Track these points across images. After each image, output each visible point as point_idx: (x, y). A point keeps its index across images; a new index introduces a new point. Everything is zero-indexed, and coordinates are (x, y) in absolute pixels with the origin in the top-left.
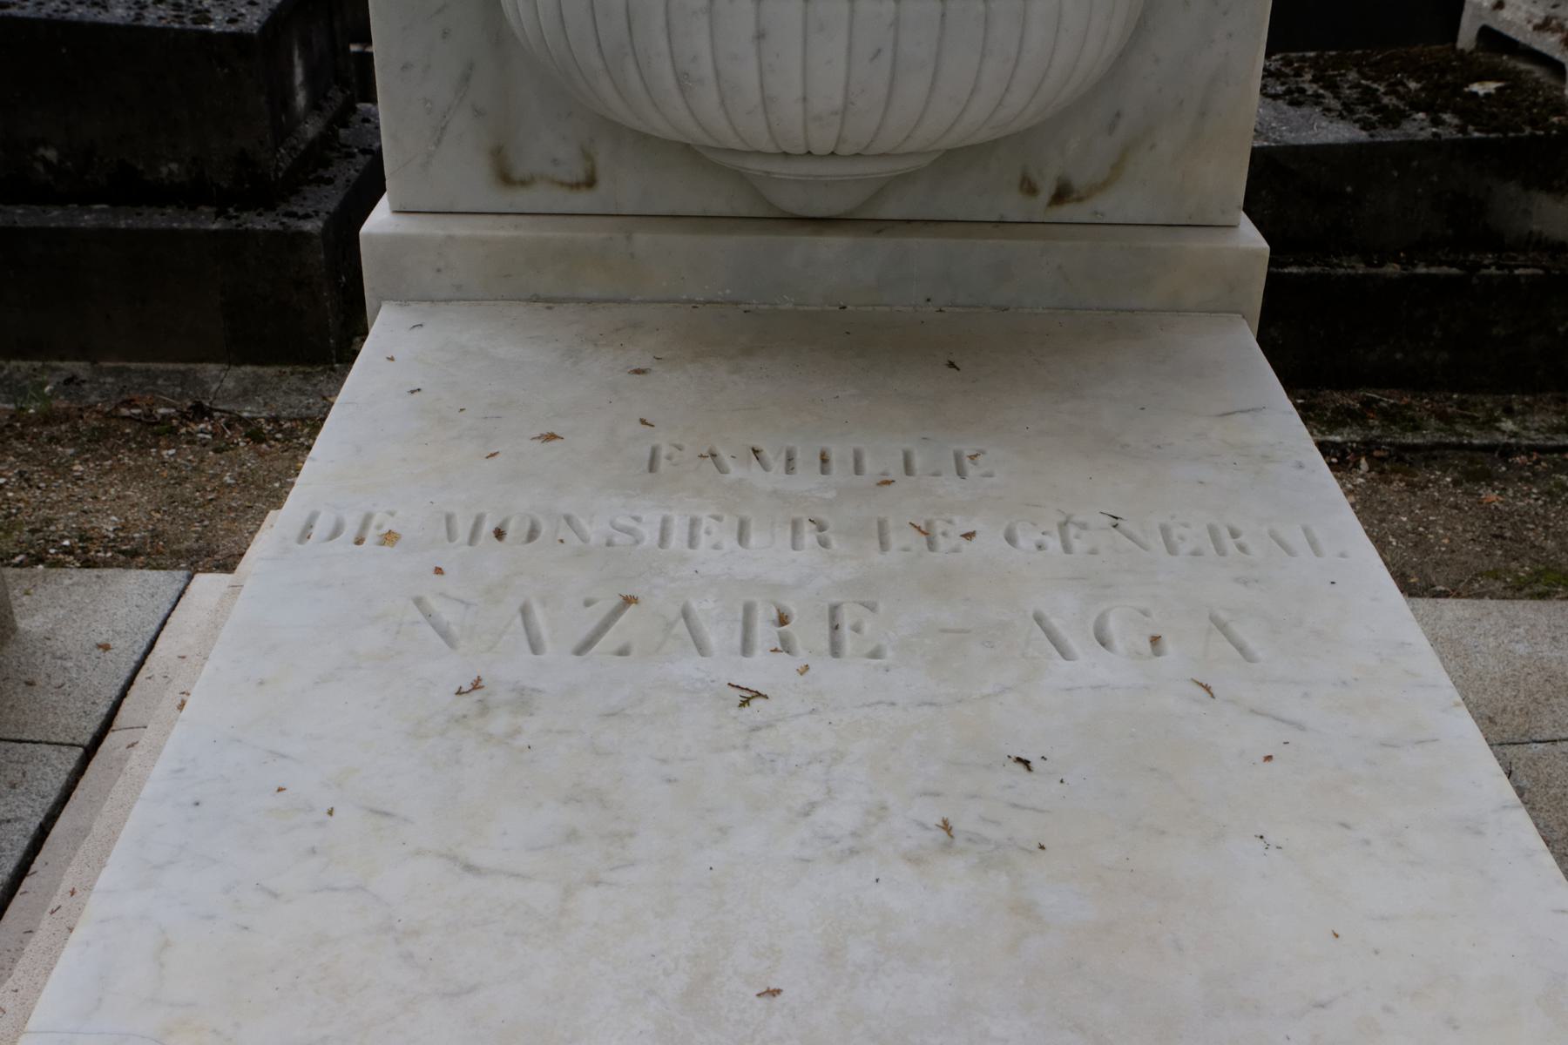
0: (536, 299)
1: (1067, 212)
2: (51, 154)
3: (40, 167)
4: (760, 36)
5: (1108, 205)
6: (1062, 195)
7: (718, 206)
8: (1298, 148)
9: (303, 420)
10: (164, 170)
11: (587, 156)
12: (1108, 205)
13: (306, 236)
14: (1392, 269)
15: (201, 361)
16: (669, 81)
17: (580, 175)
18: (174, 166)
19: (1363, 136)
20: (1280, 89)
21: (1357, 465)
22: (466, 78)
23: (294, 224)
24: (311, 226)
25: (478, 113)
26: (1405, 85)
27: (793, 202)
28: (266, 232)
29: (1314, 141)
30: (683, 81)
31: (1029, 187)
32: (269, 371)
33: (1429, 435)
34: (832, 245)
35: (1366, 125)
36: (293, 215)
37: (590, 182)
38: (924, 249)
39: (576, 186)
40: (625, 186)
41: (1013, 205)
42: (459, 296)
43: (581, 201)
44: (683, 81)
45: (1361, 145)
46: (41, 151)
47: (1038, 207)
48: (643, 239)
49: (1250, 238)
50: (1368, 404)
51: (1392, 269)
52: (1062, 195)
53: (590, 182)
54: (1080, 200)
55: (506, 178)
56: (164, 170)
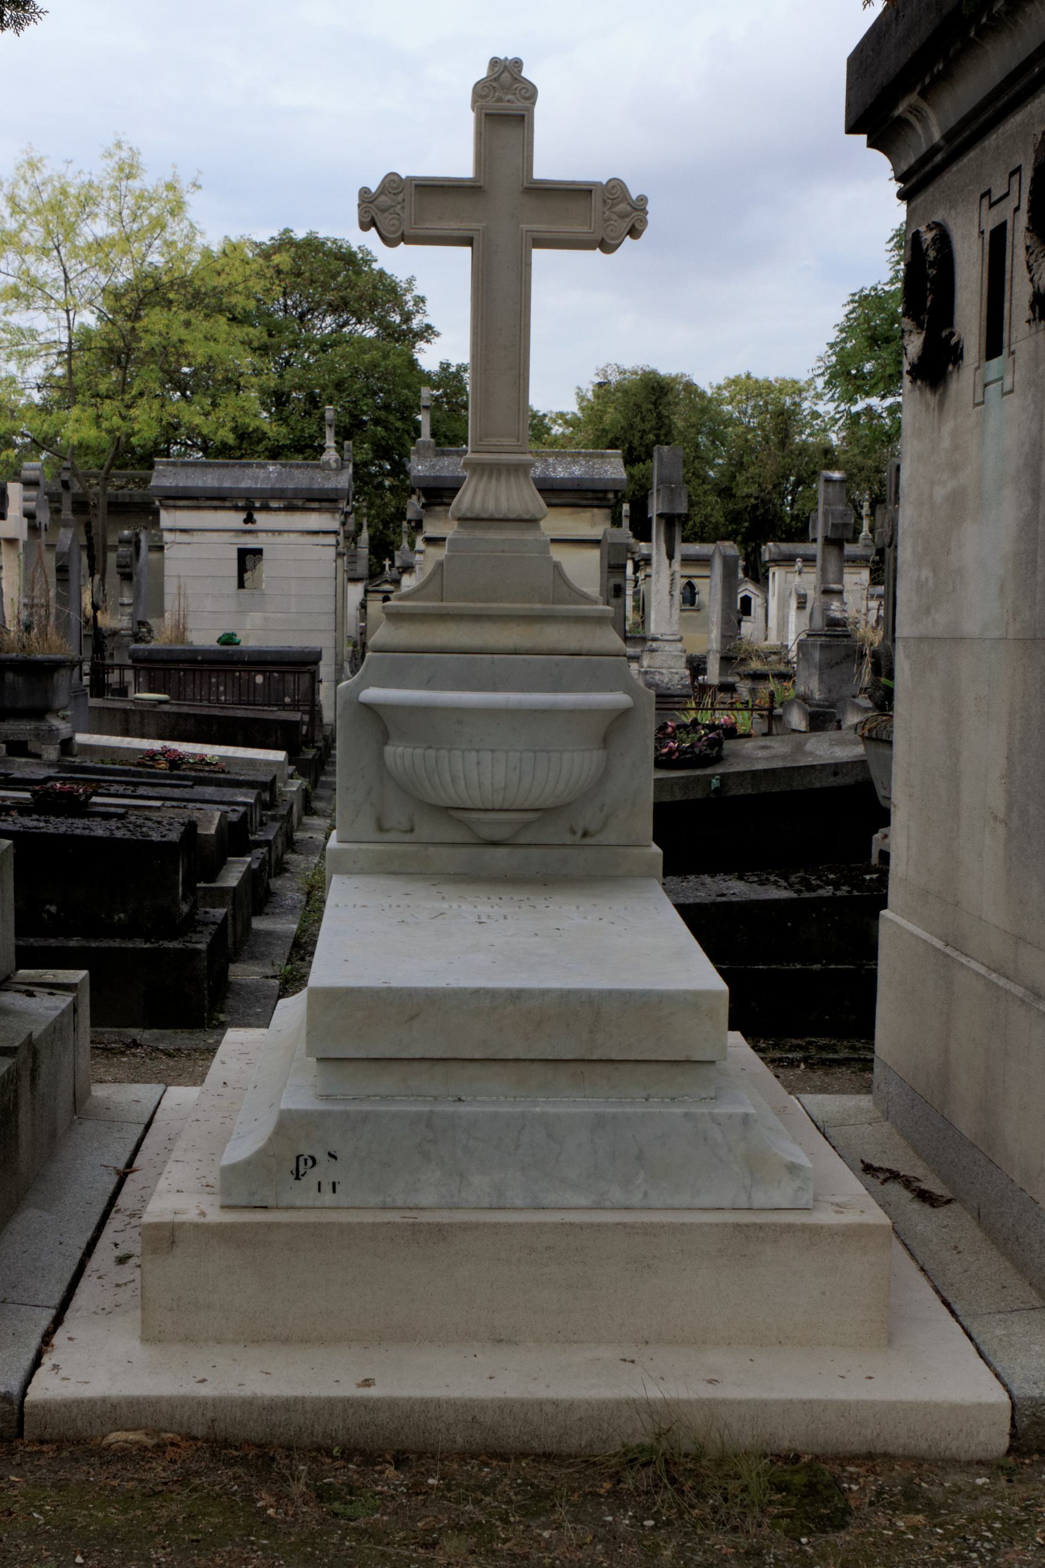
0: (390, 873)
1: (588, 841)
2: (53, 909)
3: (45, 916)
4: (478, 763)
5: (601, 838)
6: (585, 834)
7: (459, 839)
8: (758, 901)
9: (195, 1050)
10: (116, 918)
11: (411, 820)
12: (601, 838)
13: (198, 952)
14: (817, 967)
15: (127, 1027)
16: (449, 780)
17: (408, 828)
18: (122, 915)
19: (795, 895)
20: (756, 879)
21: (798, 1066)
22: (369, 793)
23: (190, 945)
24: (202, 946)
25: (372, 805)
26: (826, 876)
27: (486, 833)
28: (175, 949)
29: (767, 898)
30: (453, 779)
31: (573, 832)
32: (169, 1032)
33: (844, 1054)
34: (501, 852)
35: (798, 891)
36: (190, 942)
37: (412, 830)
38: (535, 853)
39: (406, 832)
40: (426, 830)
41: (568, 839)
42: (363, 872)
43: (408, 837)
44: (453, 779)
45: (792, 899)
46: (48, 907)
47: (577, 839)
48: (431, 850)
49: (656, 849)
50: (810, 1043)
51: (817, 967)
52: (585, 834)
53: (412, 830)
54: (592, 836)
55: (381, 828)
56: (116, 918)
